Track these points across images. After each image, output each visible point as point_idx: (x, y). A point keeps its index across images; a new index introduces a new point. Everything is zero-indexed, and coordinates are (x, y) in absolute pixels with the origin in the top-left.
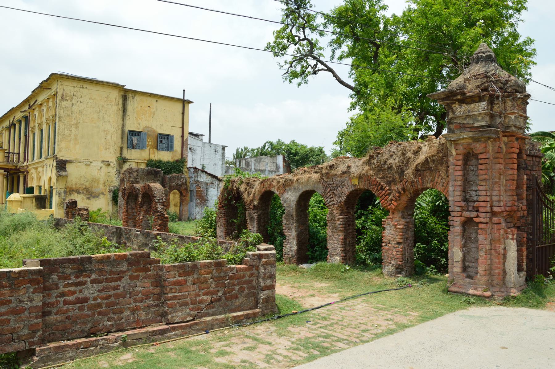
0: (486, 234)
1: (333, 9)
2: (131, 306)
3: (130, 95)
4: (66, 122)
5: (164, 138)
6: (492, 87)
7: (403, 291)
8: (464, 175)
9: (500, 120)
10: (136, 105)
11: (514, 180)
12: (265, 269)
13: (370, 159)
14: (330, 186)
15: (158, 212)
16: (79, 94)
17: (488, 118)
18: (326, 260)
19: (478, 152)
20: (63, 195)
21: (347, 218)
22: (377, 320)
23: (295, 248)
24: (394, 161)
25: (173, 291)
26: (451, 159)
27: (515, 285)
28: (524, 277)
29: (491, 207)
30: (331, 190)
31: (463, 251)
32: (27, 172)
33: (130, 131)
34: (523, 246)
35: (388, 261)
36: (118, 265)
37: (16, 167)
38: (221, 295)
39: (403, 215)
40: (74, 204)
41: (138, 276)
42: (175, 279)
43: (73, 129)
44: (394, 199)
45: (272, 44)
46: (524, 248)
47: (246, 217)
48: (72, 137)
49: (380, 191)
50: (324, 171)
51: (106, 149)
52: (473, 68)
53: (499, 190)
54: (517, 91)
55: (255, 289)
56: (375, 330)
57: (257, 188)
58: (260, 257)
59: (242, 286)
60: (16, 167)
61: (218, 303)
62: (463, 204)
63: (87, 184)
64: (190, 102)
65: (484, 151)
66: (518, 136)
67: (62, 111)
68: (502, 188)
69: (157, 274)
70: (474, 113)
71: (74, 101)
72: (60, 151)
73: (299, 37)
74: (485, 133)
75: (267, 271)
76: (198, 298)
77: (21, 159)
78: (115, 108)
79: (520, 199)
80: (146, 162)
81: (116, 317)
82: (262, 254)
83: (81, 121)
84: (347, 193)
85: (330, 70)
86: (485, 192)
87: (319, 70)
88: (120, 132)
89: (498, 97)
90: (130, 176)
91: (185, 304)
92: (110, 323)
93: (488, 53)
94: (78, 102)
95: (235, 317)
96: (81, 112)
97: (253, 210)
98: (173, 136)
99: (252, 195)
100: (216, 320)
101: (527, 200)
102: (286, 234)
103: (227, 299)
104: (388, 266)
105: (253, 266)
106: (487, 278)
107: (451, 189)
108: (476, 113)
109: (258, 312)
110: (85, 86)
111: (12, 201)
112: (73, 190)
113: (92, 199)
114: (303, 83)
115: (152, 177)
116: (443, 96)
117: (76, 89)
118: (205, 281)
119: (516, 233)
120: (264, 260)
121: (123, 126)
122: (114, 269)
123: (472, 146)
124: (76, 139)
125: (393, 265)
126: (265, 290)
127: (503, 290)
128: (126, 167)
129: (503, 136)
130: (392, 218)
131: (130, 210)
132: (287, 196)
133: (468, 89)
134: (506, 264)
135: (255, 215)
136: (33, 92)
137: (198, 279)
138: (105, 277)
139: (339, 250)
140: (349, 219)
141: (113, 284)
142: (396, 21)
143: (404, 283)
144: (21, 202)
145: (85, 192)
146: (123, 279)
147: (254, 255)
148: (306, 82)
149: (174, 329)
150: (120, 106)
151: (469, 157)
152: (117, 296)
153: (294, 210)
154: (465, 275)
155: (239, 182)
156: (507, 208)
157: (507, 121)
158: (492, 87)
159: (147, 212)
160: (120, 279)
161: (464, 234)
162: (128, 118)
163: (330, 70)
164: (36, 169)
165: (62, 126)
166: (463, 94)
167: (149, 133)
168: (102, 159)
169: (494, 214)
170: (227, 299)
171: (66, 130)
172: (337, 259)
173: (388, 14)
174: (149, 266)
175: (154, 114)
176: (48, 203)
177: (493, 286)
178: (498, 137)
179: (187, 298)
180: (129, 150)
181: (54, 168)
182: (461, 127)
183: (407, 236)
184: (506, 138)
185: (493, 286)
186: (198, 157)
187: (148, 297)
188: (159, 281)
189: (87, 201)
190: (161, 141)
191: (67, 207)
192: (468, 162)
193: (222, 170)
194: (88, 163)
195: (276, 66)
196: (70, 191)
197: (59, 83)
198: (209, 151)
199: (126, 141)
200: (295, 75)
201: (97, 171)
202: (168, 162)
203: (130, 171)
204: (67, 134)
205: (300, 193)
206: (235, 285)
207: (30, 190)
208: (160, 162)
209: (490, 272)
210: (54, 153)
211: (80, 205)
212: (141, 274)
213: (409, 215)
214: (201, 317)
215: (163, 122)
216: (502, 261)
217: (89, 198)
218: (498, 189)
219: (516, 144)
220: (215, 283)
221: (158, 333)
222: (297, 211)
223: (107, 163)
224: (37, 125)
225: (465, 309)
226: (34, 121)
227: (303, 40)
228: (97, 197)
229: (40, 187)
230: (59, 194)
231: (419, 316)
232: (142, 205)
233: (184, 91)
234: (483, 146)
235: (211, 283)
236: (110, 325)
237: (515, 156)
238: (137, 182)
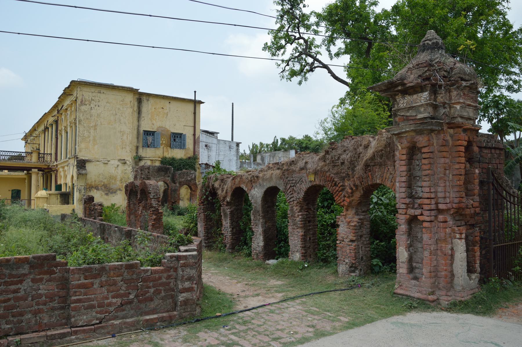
0: (431, 233)
1: (325, 7)
2: (33, 308)
3: (144, 98)
4: (85, 125)
5: (177, 137)
6: (435, 76)
7: (350, 292)
8: (409, 170)
9: (444, 111)
10: (150, 106)
11: (461, 175)
12: (183, 271)
13: (325, 154)
14: (290, 182)
15: (152, 207)
16: (97, 98)
17: (430, 109)
18: (288, 256)
19: (421, 146)
20: (83, 191)
21: (306, 215)
22: (298, 326)
23: (262, 244)
24: (346, 157)
25: (78, 294)
26: (397, 153)
27: (463, 289)
28: (477, 280)
29: (437, 204)
30: (291, 186)
31: (409, 251)
32: (57, 171)
33: (145, 131)
34: (475, 246)
35: (342, 259)
36: (19, 268)
37: (49, 166)
38: (133, 297)
39: (357, 212)
40: (91, 199)
41: (41, 280)
42: (80, 282)
43: (92, 131)
44: (347, 195)
45: (269, 44)
46: (477, 248)
47: (221, 213)
48: (91, 138)
49: (334, 188)
50: (285, 167)
51: (122, 148)
52: (418, 56)
53: (445, 186)
54: (462, 79)
55: (173, 291)
56: (288, 338)
57: (229, 185)
58: (178, 258)
59: (158, 288)
60: (49, 166)
61: (129, 306)
62: (408, 201)
63: (105, 181)
64: (201, 102)
65: (427, 145)
66: (465, 127)
67: (82, 115)
68: (448, 184)
69: (63, 277)
70: (416, 105)
71: (92, 106)
72: (80, 151)
73: (295, 37)
74: (431, 125)
75: (185, 273)
76: (106, 301)
77: (53, 159)
78: (130, 110)
79: (469, 193)
80: (160, 159)
81: (15, 320)
82: (180, 256)
83: (99, 124)
84: (305, 189)
85: (325, 66)
86: (428, 189)
87: (315, 67)
88: (135, 132)
89: (440, 86)
90: (142, 173)
91: (92, 307)
92: (8, 326)
93: (435, 41)
94: (96, 106)
95: (147, 320)
96: (98, 115)
97: (227, 205)
98: (185, 135)
99: (224, 192)
100: (125, 323)
101: (479, 195)
102: (254, 230)
103: (140, 301)
104: (342, 264)
105: (171, 268)
106: (432, 280)
107: (397, 184)
108: (418, 104)
109: (175, 315)
110: (102, 92)
111: (39, 198)
112: (92, 187)
113: (110, 195)
114: (303, 80)
115: (163, 173)
116: (383, 88)
117: (94, 94)
118: (115, 284)
119: (464, 232)
120: (181, 262)
121: (139, 126)
122: (14, 273)
123: (415, 140)
124: (94, 140)
125: (347, 263)
126: (184, 292)
127: (450, 293)
128: (142, 163)
129: (449, 128)
130: (345, 215)
131: (132, 205)
132: (254, 192)
133: (410, 80)
134: (454, 265)
135: (228, 211)
136: (59, 98)
137: (106, 281)
138: (3, 281)
139: (299, 247)
140: (309, 216)
141: (13, 287)
142: (385, 14)
143: (354, 283)
144: (47, 198)
145: (103, 188)
146: (25, 282)
147: (171, 257)
148: (306, 79)
149: (76, 333)
150: (136, 108)
151: (413, 151)
152: (17, 299)
153: (260, 206)
154: (411, 276)
155: (214, 179)
156: (454, 205)
157: (452, 111)
158: (435, 76)
159: (145, 208)
160: (21, 282)
161: (410, 233)
162: (143, 119)
163: (325, 66)
164: (63, 167)
165: (82, 129)
166: (404, 84)
167: (163, 132)
168: (119, 158)
169: (440, 211)
170: (140, 301)
171: (85, 132)
172: (297, 256)
173: (378, 10)
174: (55, 269)
175: (167, 115)
176: (72, 199)
177: (439, 289)
178: (443, 129)
179: (93, 301)
180: (145, 149)
181: (75, 167)
182: (404, 120)
183: (360, 233)
184: (452, 130)
185: (439, 289)
186: (213, 154)
187: (52, 300)
188: (64, 284)
189: (106, 197)
190: (175, 140)
191: (85, 202)
192: (414, 157)
193: (237, 165)
194: (106, 162)
195: (270, 67)
196: (90, 187)
197: (79, 89)
198: (224, 148)
199: (141, 141)
200: (293, 73)
201: (114, 169)
202: (181, 159)
203: (142, 168)
204: (87, 136)
205: (265, 189)
206: (150, 288)
207: (59, 187)
208: (173, 159)
209: (435, 273)
210: (75, 153)
211: (96, 201)
212: (45, 277)
213: (363, 212)
214: (110, 320)
215: (176, 122)
216: (449, 262)
217: (107, 194)
218: (444, 183)
219: (463, 136)
220: (126, 285)
221: (57, 337)
222: (263, 206)
223: (123, 162)
224: (63, 128)
225: (401, 314)
226: (62, 125)
227: (299, 39)
228: (115, 192)
229: (66, 184)
230: (80, 190)
231: (348, 322)
232: (140, 201)
233: (195, 92)
234: (426, 139)
235: (122, 286)
236: (9, 328)
237: (462, 149)
238: (149, 179)
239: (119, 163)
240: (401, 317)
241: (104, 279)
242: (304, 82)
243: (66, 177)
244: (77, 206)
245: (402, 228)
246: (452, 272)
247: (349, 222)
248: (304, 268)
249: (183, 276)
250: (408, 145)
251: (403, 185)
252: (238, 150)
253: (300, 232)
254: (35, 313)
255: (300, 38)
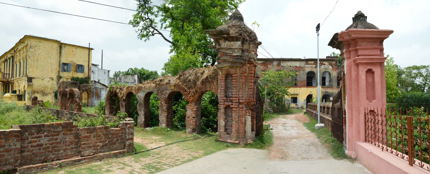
8: (225, 85)
23: (143, 120)
24: (192, 78)
26: (219, 77)
29: (239, 100)
32: (13, 83)
33: (63, 63)
40: (36, 98)
41: (67, 134)
43: (36, 62)
45: (132, 21)
46: (255, 120)
48: (35, 66)
50: (158, 83)
57: (125, 91)
58: (126, 124)
62: (225, 98)
63: (42, 89)
64: (92, 49)
71: (36, 49)
72: (29, 73)
78: (56, 52)
81: (56, 153)
84: (169, 93)
85: (160, 33)
88: (58, 63)
91: (90, 147)
95: (114, 153)
96: (39, 54)
105: (123, 128)
106: (237, 134)
107: (219, 91)
117: (37, 43)
118: (100, 136)
121: (60, 60)
122: (56, 130)
124: (37, 67)
127: (244, 140)
128: (61, 80)
131: (63, 102)
135: (124, 104)
137: (96, 135)
141: (55, 137)
147: (123, 123)
149: (84, 159)
150: (59, 51)
151: (228, 76)
152: (57, 143)
154: (226, 133)
156: (246, 101)
160: (58, 135)
161: (226, 113)
163: (160, 33)
164: (18, 81)
165: (30, 61)
169: (240, 103)
170: (110, 144)
172: (164, 125)
191: (33, 100)
195: (134, 32)
196: (34, 92)
197: (29, 40)
198: (101, 73)
200: (143, 36)
202: (82, 78)
203: (63, 83)
206: (114, 138)
207: (15, 92)
208: (78, 78)
209: (238, 131)
211: (39, 99)
212: (69, 132)
215: (80, 59)
217: (43, 96)
222: (144, 102)
227: (147, 19)
232: (69, 99)
234: (235, 70)
238: (67, 88)
239: (49, 80)
240: (225, 150)
241: (95, 133)
242: (147, 41)
243: (19, 86)
244: (27, 102)
245: (222, 110)
246: (245, 130)
247: (192, 109)
248: (168, 131)
249: (129, 133)
250: (226, 73)
251: (223, 91)
252: (108, 74)
253: (165, 114)
254: (65, 150)
255: (148, 18)
